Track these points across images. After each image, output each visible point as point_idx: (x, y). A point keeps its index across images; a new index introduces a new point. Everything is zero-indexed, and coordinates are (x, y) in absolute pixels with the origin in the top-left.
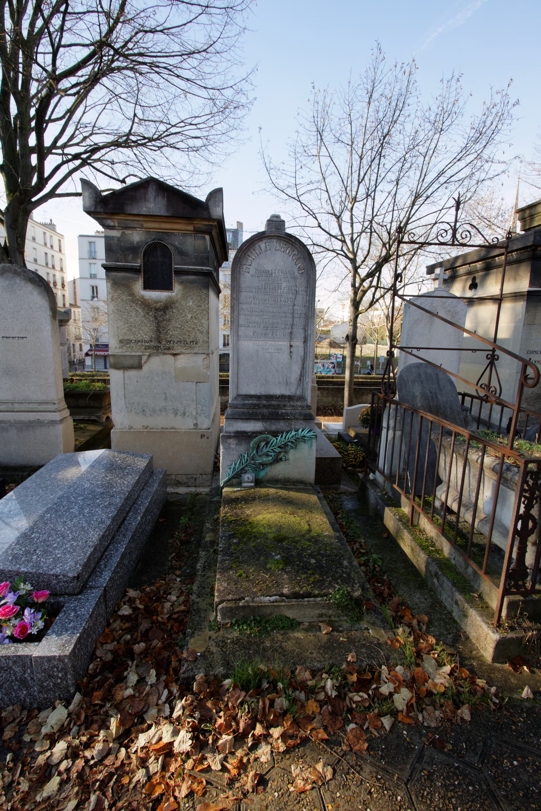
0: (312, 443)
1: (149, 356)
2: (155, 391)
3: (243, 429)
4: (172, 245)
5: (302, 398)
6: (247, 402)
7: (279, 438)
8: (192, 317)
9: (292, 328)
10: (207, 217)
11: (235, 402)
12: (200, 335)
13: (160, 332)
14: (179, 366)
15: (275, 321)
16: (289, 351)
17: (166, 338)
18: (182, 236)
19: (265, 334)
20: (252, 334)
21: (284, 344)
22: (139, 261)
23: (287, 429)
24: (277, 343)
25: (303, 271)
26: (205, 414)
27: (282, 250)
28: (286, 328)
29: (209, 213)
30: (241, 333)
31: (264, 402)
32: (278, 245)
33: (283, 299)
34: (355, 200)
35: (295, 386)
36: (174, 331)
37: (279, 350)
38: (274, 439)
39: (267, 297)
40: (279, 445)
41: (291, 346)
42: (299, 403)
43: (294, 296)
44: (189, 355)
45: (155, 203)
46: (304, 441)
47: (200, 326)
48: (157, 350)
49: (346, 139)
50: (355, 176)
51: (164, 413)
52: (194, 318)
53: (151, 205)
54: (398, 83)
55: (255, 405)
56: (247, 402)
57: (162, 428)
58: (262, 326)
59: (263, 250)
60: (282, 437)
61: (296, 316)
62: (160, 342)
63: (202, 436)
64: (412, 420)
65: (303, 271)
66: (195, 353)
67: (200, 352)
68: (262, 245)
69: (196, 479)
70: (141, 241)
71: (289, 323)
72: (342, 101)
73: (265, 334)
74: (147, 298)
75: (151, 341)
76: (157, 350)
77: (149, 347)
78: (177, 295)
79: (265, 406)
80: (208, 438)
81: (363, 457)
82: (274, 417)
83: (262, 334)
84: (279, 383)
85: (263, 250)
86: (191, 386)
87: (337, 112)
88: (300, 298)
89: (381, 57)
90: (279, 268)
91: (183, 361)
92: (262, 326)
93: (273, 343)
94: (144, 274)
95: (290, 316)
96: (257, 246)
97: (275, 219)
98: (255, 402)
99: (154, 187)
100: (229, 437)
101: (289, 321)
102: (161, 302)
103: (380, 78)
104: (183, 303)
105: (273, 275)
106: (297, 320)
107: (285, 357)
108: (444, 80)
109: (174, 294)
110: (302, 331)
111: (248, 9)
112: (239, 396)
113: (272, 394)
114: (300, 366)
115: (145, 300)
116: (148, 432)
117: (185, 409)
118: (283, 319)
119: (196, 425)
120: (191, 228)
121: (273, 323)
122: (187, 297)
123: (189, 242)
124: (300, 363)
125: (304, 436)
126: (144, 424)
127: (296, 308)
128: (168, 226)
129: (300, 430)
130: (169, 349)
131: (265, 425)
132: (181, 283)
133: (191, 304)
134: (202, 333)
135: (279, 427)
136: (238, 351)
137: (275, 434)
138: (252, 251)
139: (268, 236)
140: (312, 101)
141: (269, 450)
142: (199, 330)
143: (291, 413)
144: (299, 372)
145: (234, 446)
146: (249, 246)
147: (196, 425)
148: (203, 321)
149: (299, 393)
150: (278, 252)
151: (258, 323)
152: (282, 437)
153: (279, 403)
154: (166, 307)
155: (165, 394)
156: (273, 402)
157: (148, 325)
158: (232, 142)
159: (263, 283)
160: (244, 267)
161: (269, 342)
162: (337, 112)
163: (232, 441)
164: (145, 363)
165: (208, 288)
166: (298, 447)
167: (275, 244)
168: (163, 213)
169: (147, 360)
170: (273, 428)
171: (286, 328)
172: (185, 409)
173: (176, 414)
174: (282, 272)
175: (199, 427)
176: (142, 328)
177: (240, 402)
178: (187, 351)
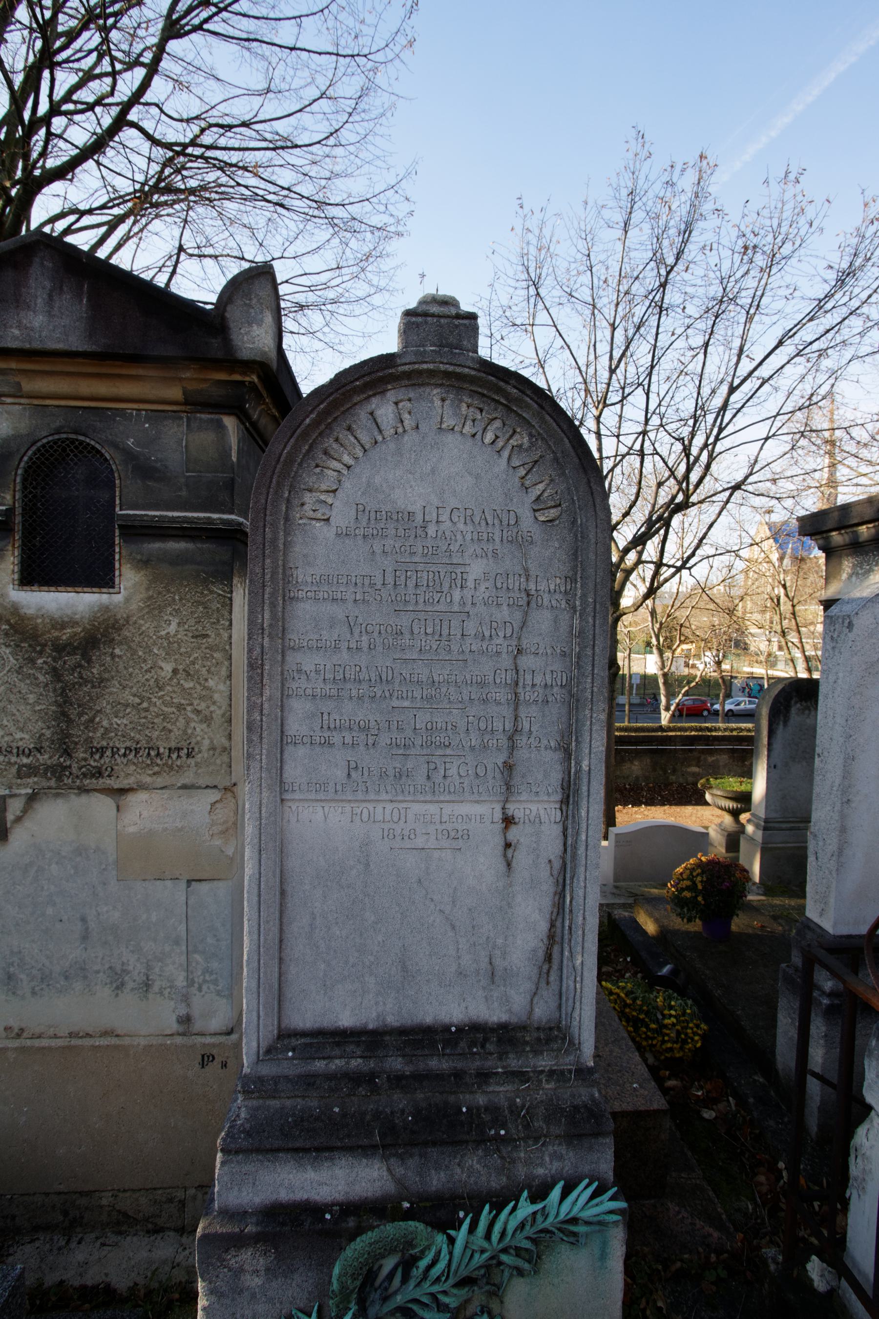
0: (604, 1244)
1: (32, 798)
2: (50, 911)
3: (300, 1195)
4: (115, 446)
5: (555, 1035)
6: (319, 1065)
7: (461, 1235)
8: (175, 671)
9: (512, 748)
10: (220, 355)
11: (267, 1070)
12: (200, 728)
13: (70, 721)
14: (132, 829)
15: (440, 720)
16: (499, 841)
17: (89, 740)
18: (148, 419)
19: (399, 776)
20: (340, 774)
21: (480, 813)
22: (9, 497)
23: (496, 1182)
24: (448, 809)
25: (553, 513)
26: (215, 982)
27: (467, 429)
28: (485, 747)
29: (227, 342)
30: (293, 772)
31: (396, 1064)
32: (448, 411)
33: (471, 627)
34: (604, 403)
35: (528, 986)
36: (116, 715)
37: (458, 838)
38: (440, 1239)
39: (404, 621)
40: (463, 1273)
41: (508, 821)
42: (545, 1062)
43: (518, 615)
44: (166, 793)
45: (50, 314)
46: (574, 1239)
47: (201, 698)
48: (59, 779)
49: (585, 294)
50: (604, 361)
51: (78, 986)
52: (181, 675)
53: (37, 320)
54: (677, 198)
55: (356, 1079)
56: (319, 1065)
57: (71, 1035)
58: (384, 739)
59: (389, 432)
60: (472, 1229)
61: (526, 695)
62: (67, 753)
63: (206, 1059)
64: (356, 438)
65: (553, 513)
66: (184, 787)
67: (202, 782)
68: (385, 410)
69: (182, 1203)
70: (15, 437)
71: (498, 725)
72: (573, 232)
73: (399, 776)
74: (31, 612)
75: (39, 750)
76: (59, 779)
77: (32, 771)
78: (127, 600)
79: (398, 1081)
80: (224, 1065)
81: (703, 1037)
82: (442, 1127)
83: (383, 775)
84: (460, 974)
85: (389, 432)
86: (172, 893)
87: (566, 252)
88: (542, 620)
89: (645, 153)
90: (453, 503)
91: (148, 812)
92: (384, 739)
93: (433, 808)
94: (24, 537)
95: (503, 695)
96: (362, 414)
97: (435, 309)
98: (355, 1063)
99: (48, 264)
100: (237, 1242)
101: (500, 717)
102: (74, 623)
103: (646, 187)
104: (147, 625)
105: (431, 530)
106: (534, 710)
107: (484, 862)
108: (771, 180)
109: (118, 598)
110: (552, 759)
111: (397, 62)
112: (286, 1036)
113: (429, 1020)
114: (547, 902)
115: (22, 618)
116: (23, 1050)
117: (149, 968)
118: (472, 711)
119: (186, 1020)
120: (175, 393)
121: (431, 729)
122: (161, 609)
123: (161, 430)
124: (548, 887)
125: (574, 1221)
126: (11, 1022)
127: (526, 662)
128: (102, 388)
129: (556, 1193)
130: (98, 773)
131: (400, 1171)
132: (143, 563)
133: (172, 628)
134: (207, 720)
135: (459, 1174)
136: (282, 852)
137: (441, 1212)
138: (344, 435)
139: (408, 375)
140: (519, 230)
141: (417, 1294)
142: (198, 712)
143: (514, 1110)
144: (543, 927)
145: (258, 1281)
146: (327, 412)
147: (186, 1020)
148: (211, 683)
149: (542, 1012)
150: (450, 438)
151: (365, 729)
152: (472, 1229)
153: (459, 1065)
154: (94, 640)
155: (83, 920)
156: (434, 1063)
157: (32, 698)
158: (374, 314)
159: (388, 564)
160: (308, 498)
161: (416, 808)
162: (566, 252)
163: (249, 1259)
164: (18, 819)
165: (230, 580)
166: (548, 1263)
167: (436, 406)
168: (76, 342)
169: (25, 811)
170: (436, 1181)
171: (485, 747)
172: (149, 968)
173: (120, 987)
174: (469, 519)
175: (198, 1026)
176: (11, 708)
177: (289, 1066)
178: (160, 781)
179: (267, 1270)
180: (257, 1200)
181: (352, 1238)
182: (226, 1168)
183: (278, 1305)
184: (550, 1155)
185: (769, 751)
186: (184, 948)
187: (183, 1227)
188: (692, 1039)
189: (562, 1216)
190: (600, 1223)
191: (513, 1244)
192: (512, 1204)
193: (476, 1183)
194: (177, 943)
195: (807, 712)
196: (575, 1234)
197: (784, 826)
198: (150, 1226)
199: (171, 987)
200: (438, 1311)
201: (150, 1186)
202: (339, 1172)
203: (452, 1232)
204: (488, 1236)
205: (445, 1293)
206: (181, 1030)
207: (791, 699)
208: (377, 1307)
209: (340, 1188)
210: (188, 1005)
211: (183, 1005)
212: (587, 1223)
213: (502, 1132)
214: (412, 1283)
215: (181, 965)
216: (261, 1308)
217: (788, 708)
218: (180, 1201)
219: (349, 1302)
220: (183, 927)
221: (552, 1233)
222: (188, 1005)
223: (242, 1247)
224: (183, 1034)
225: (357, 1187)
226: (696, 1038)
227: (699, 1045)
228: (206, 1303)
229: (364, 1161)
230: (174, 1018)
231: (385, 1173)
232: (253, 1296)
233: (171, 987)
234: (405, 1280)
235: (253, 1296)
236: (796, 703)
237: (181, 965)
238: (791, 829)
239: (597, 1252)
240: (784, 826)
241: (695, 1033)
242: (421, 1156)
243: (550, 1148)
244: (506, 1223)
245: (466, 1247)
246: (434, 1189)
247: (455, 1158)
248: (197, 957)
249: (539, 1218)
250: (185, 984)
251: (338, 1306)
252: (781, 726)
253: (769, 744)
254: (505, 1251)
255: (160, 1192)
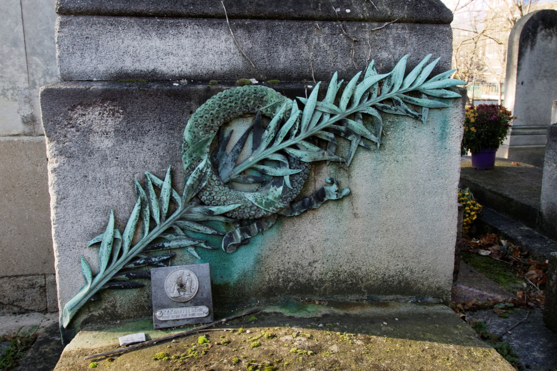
0: (445, 124)
7: (310, 102)
38: (289, 103)
40: (314, 129)
60: (322, 95)
125: (417, 93)
131: (247, 44)
135: (307, 53)
141: (270, 154)
152: (322, 95)
170: (284, 58)
179: (117, 131)
180: (102, 68)
181: (202, 100)
182: (66, 30)
183: (130, 169)
184: (394, 39)
185: (518, 70)
186: (23, 50)
187: (46, 309)
188: (469, 214)
189: (406, 86)
190: (441, 98)
191: (361, 109)
192: (359, 74)
193: (322, 63)
194: (15, 44)
195: (549, 38)
196: (418, 107)
197: (527, 131)
198: (16, 309)
199: (13, 89)
200: (290, 168)
201: (12, 274)
202: (186, 42)
203: (302, 99)
204: (337, 102)
205: (295, 146)
206: (27, 130)
207: (538, 26)
208: (230, 168)
209: (187, 59)
210: (32, 106)
211: (27, 106)
212: (429, 97)
213: (348, 11)
214: (264, 145)
215: (21, 67)
216: (112, 171)
217: (535, 34)
218: (41, 287)
219: (202, 153)
220: (20, 28)
221: (398, 103)
222: (32, 106)
223: (90, 105)
224: (30, 134)
225: (204, 59)
226: (473, 213)
227: (474, 218)
228: (56, 165)
229: (211, 30)
230: (19, 119)
231: (232, 46)
232: (105, 158)
233: (13, 89)
234: (256, 145)
235: (105, 158)
236: (542, 29)
237: (21, 67)
238: (532, 134)
239: (438, 131)
240: (527, 131)
241: (472, 210)
242: (268, 29)
243: (394, 31)
244: (354, 90)
245: (315, 110)
246: (281, 66)
247: (302, 34)
248: (36, 59)
249: (386, 88)
250: (27, 85)
251: (191, 156)
252: (529, 50)
253: (519, 64)
254: (354, 116)
255: (22, 279)
